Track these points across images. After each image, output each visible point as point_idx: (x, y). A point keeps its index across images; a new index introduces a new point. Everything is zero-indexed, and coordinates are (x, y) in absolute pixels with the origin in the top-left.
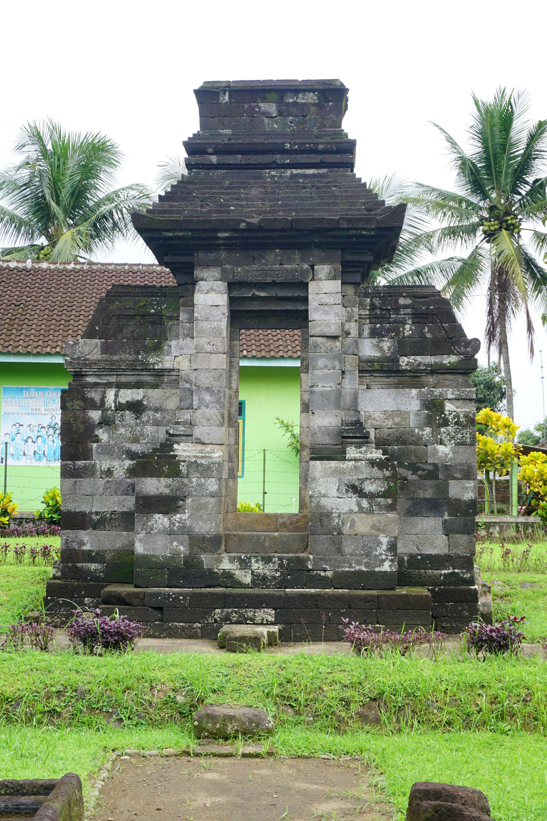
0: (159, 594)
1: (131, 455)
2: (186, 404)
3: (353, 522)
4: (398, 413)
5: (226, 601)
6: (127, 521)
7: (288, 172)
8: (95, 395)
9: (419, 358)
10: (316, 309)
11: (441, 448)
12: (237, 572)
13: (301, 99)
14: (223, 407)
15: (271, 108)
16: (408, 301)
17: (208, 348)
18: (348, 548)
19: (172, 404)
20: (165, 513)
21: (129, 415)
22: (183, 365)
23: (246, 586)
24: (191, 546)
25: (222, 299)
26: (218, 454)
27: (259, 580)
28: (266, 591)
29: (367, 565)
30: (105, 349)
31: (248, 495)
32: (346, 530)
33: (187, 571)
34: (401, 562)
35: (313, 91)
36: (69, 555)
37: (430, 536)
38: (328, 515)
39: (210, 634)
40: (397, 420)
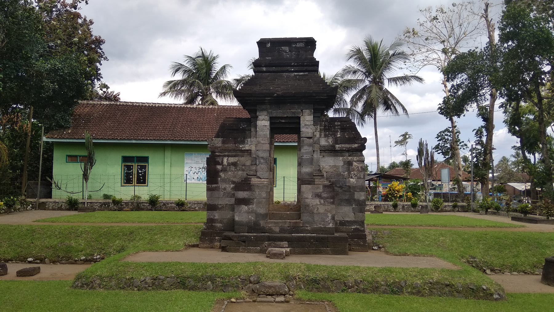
0: (243, 236)
1: (233, 182)
2: (254, 163)
3: (318, 209)
4: (335, 166)
5: (269, 239)
6: (232, 208)
7: (293, 74)
8: (219, 159)
9: (343, 145)
10: (303, 127)
11: (351, 180)
12: (273, 228)
13: (298, 45)
14: (268, 164)
15: (287, 49)
16: (339, 123)
17: (263, 142)
18: (316, 218)
19: (248, 163)
20: (246, 205)
21: (233, 168)
22: (253, 148)
23: (275, 233)
24: (256, 217)
25: (267, 123)
26: (265, 182)
27: (282, 230)
28: (285, 235)
29: (323, 225)
30: (223, 142)
31: (278, 196)
32: (315, 211)
33: (254, 227)
34: (336, 224)
35: (302, 42)
36: (210, 221)
37: (347, 213)
38: (308, 206)
39: (263, 251)
40: (335, 169)
